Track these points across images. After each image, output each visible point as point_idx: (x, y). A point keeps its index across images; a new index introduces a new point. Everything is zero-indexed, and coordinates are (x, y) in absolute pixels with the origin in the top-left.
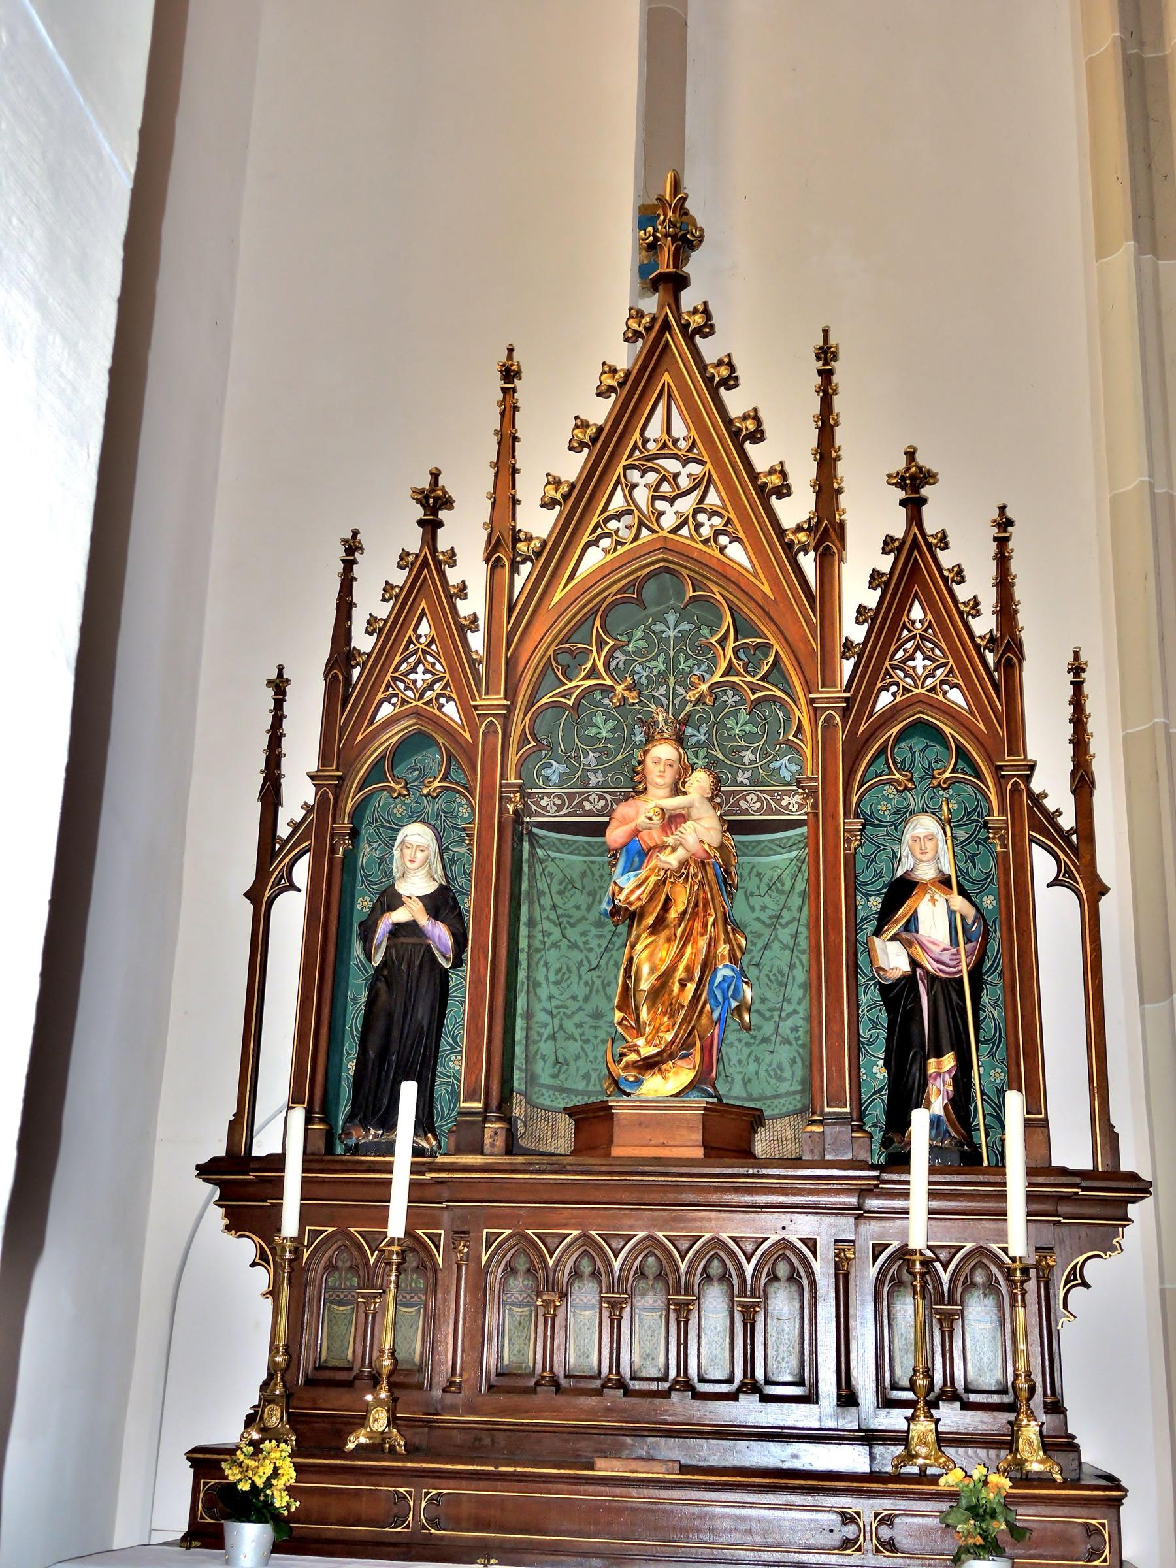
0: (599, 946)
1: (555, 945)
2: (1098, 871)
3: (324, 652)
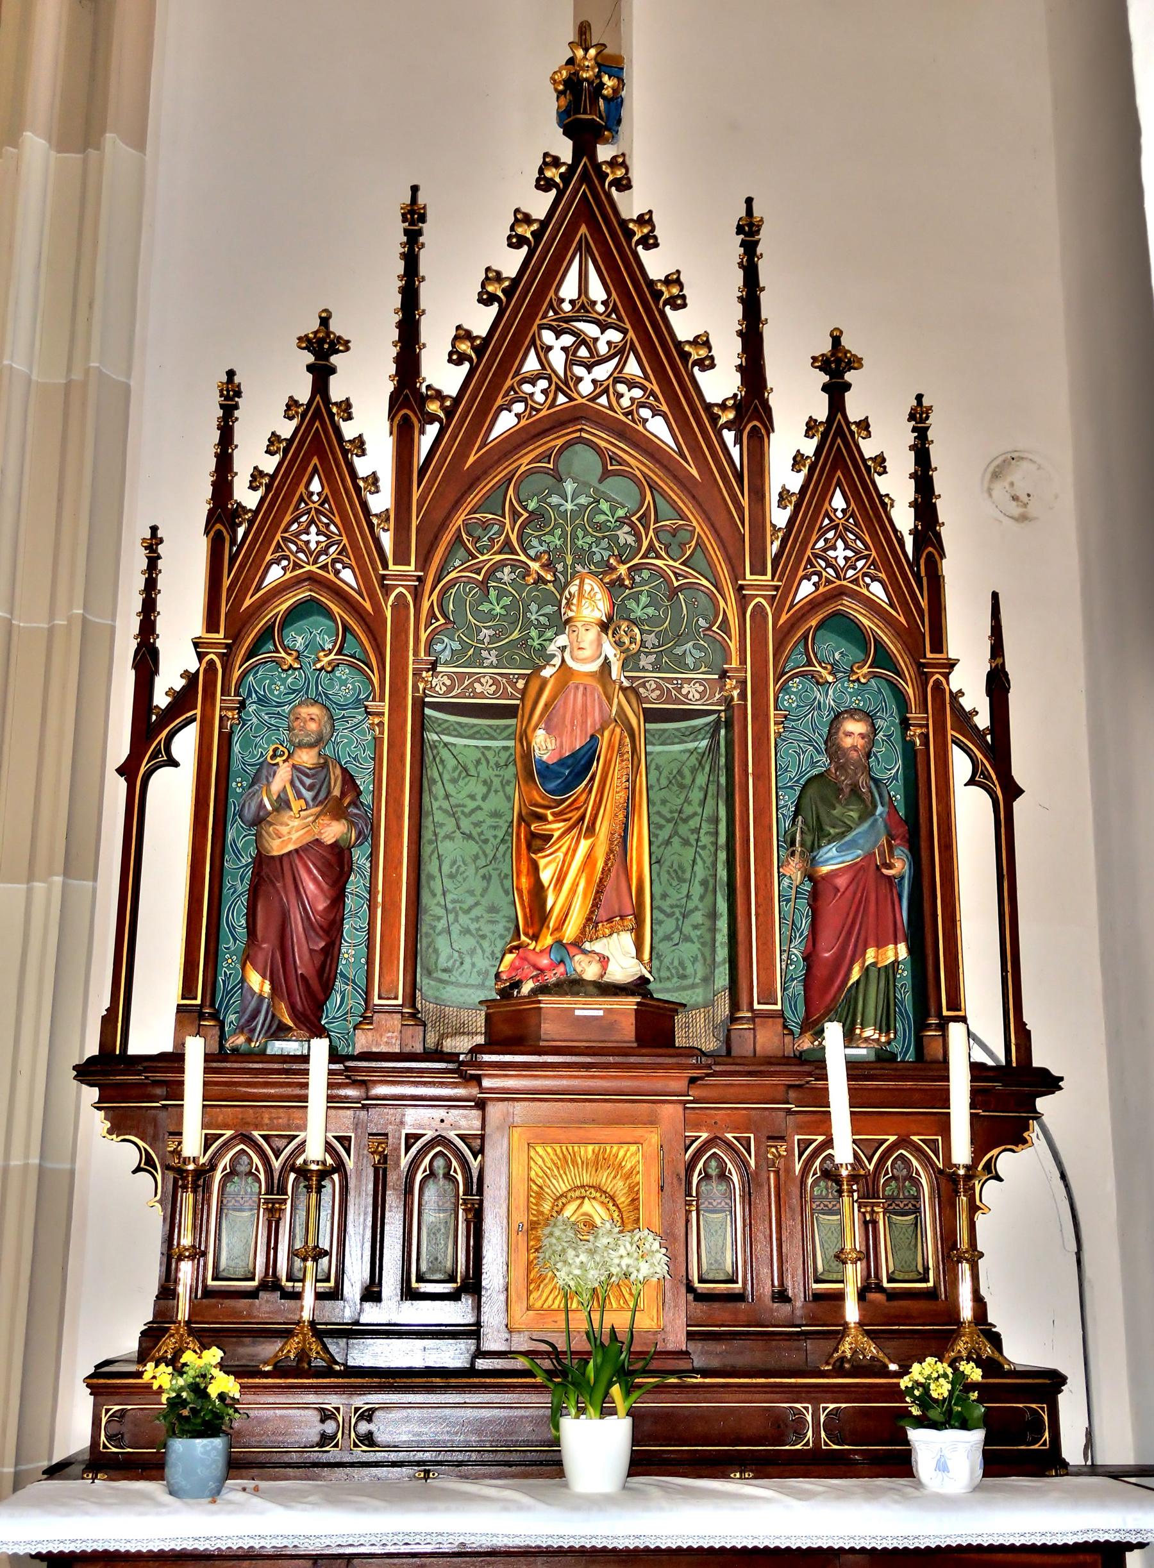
0: (495, 837)
1: (449, 837)
2: (1013, 774)
3: (203, 509)
